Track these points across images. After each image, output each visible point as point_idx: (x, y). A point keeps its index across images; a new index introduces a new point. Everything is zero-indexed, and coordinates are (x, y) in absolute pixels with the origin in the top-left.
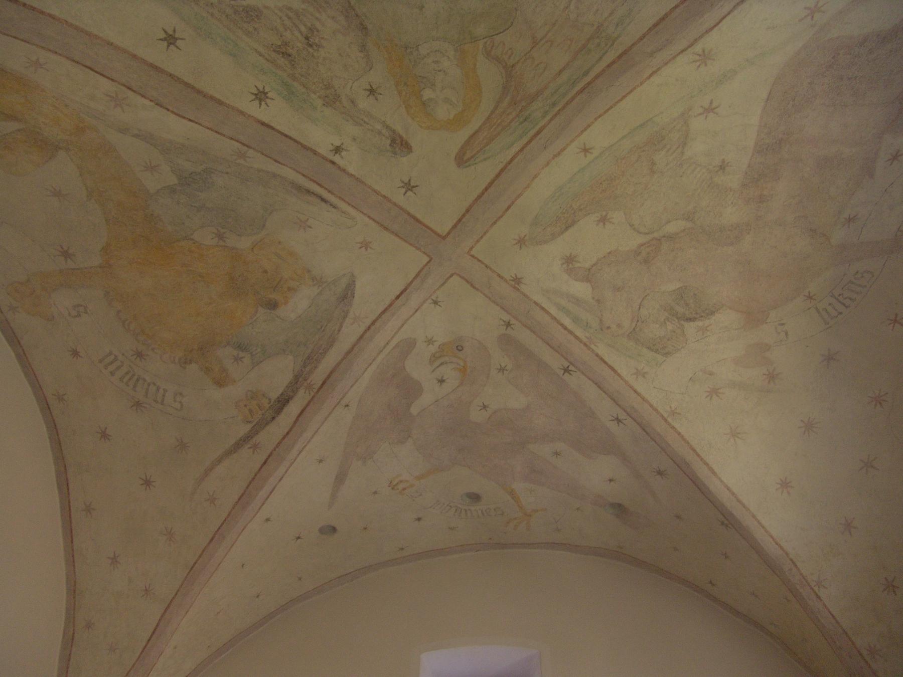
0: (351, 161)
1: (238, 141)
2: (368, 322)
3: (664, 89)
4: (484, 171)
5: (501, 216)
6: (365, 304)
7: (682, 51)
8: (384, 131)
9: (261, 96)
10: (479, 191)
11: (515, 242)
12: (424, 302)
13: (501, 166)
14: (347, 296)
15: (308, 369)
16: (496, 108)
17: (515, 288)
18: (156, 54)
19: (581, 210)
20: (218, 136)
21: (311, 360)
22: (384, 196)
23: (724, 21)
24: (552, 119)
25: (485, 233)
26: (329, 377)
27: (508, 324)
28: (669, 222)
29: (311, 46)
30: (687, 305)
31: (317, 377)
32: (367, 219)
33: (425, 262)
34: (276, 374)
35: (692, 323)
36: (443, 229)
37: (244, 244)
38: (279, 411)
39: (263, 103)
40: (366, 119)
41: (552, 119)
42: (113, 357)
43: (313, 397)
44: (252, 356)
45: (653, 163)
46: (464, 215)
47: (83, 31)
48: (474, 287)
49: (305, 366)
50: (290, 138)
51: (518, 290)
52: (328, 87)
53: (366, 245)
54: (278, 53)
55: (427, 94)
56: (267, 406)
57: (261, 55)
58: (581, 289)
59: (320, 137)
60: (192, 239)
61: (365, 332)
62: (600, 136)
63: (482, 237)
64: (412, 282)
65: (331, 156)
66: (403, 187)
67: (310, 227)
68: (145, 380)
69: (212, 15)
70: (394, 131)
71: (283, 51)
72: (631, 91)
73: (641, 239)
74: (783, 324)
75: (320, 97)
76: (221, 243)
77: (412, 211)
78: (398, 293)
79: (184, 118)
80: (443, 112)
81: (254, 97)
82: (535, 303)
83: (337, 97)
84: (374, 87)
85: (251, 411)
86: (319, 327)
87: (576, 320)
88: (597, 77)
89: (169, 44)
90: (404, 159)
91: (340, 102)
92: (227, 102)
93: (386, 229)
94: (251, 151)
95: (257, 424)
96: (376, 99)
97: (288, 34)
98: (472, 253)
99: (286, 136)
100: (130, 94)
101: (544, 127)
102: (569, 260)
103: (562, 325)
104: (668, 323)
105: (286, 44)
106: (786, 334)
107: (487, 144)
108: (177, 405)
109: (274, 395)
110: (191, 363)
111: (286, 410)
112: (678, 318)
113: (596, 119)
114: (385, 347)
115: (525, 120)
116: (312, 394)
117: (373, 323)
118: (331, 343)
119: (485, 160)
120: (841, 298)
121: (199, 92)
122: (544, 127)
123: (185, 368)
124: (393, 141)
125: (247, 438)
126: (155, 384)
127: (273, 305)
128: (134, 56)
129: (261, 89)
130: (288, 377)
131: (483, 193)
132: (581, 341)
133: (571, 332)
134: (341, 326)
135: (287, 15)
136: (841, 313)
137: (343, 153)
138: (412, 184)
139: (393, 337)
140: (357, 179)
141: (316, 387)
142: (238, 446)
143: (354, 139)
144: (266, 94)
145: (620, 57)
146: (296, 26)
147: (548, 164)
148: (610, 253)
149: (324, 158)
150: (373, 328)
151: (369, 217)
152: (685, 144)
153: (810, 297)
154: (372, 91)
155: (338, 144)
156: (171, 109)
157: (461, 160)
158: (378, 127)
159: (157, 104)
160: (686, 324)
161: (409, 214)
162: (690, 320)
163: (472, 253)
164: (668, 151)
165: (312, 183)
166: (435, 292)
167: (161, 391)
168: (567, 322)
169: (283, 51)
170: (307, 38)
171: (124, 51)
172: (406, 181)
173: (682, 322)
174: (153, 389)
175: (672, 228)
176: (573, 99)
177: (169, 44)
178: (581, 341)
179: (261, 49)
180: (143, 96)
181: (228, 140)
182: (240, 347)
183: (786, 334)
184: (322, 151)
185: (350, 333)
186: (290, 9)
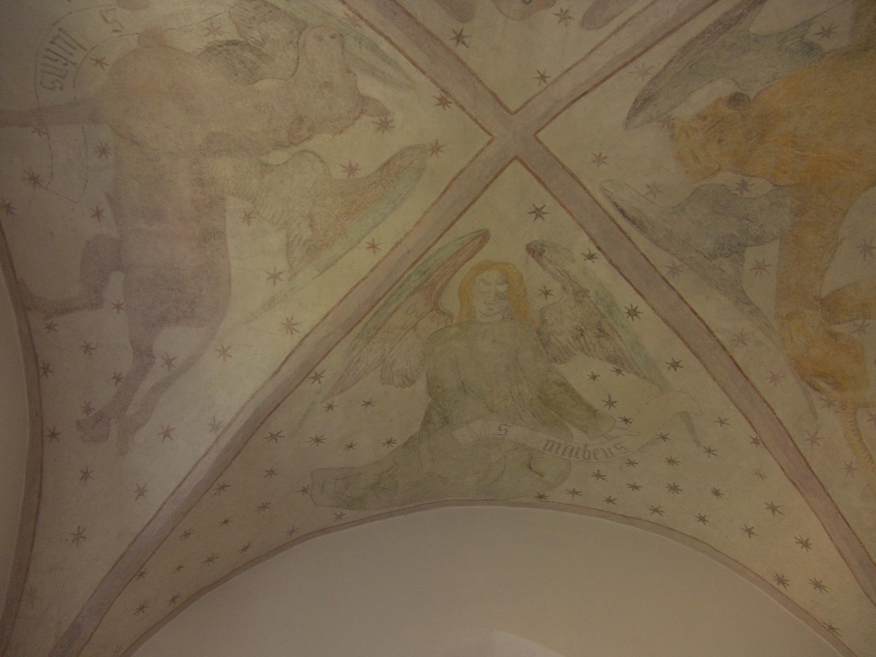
0: (583, 244)
1: (670, 285)
2: (631, 68)
3: (316, 299)
4: (465, 227)
5: (454, 179)
6: (629, 85)
7: (307, 336)
10: (473, 207)
11: (442, 149)
12: (556, 80)
13: (449, 232)
14: (644, 101)
16: (449, 280)
17: (446, 93)
19: (375, 183)
21: (726, 24)
22: (564, 207)
23: (283, 359)
24: (403, 276)
25: (472, 161)
27: (459, 38)
28: (285, 163)
29: (581, 330)
30: (242, 62)
32: (589, 188)
33: (543, 133)
35: (230, 38)
36: (517, 165)
37: (728, 178)
40: (558, 274)
41: (403, 276)
45: (311, 226)
46: (491, 182)
48: (494, 94)
50: (625, 278)
51: (443, 90)
53: (599, 159)
54: (606, 334)
55: (503, 288)
58: (371, 88)
59: (601, 270)
60: (776, 186)
61: (639, 55)
62: (361, 261)
63: (477, 156)
64: (563, 110)
67: (648, 186)
70: (538, 261)
71: (602, 333)
72: (341, 301)
73: (310, 145)
74: (116, 31)
76: (746, 179)
77: (542, 188)
78: (583, 98)
79: (699, 318)
80: (493, 275)
82: (423, 72)
87: (375, 48)
88: (368, 312)
89: (677, 363)
90: (536, 238)
92: (660, 319)
93: (572, 175)
94: (664, 274)
97: (594, 341)
98: (489, 138)
99: (628, 281)
100: (726, 344)
101: (410, 268)
102: (385, 126)
103: (391, 43)
104: (260, 39)
106: (105, 20)
107: (459, 251)
112: (248, 45)
113: (366, 277)
115: (425, 272)
117: (625, 65)
118: (685, 49)
119: (463, 237)
120: (64, 62)
122: (410, 268)
124: (540, 254)
127: (736, 100)
131: (469, 206)
132: (366, 21)
133: (381, 33)
134: (666, 67)
136: (52, 42)
137: (588, 253)
138: (534, 215)
139: (609, 37)
140: (583, 228)
144: (629, 313)
145: (352, 329)
147: (407, 235)
148: (341, 132)
150: (628, 59)
151: (585, 189)
152: (287, 245)
153: (99, 62)
154: (547, 293)
157: (484, 236)
158: (550, 266)
159: (712, 333)
160: (237, 37)
161: (545, 187)
162: (234, 43)
163: (489, 138)
164: (301, 239)
166: (540, 93)
168: (385, 46)
169: (602, 333)
170: (582, 335)
171: (709, 372)
172: (539, 219)
173: (242, 39)
175: (279, 157)
176: (385, 294)
178: (366, 21)
180: (718, 341)
182: (810, 48)
183: (105, 20)
185: (657, 59)
186: (586, 354)
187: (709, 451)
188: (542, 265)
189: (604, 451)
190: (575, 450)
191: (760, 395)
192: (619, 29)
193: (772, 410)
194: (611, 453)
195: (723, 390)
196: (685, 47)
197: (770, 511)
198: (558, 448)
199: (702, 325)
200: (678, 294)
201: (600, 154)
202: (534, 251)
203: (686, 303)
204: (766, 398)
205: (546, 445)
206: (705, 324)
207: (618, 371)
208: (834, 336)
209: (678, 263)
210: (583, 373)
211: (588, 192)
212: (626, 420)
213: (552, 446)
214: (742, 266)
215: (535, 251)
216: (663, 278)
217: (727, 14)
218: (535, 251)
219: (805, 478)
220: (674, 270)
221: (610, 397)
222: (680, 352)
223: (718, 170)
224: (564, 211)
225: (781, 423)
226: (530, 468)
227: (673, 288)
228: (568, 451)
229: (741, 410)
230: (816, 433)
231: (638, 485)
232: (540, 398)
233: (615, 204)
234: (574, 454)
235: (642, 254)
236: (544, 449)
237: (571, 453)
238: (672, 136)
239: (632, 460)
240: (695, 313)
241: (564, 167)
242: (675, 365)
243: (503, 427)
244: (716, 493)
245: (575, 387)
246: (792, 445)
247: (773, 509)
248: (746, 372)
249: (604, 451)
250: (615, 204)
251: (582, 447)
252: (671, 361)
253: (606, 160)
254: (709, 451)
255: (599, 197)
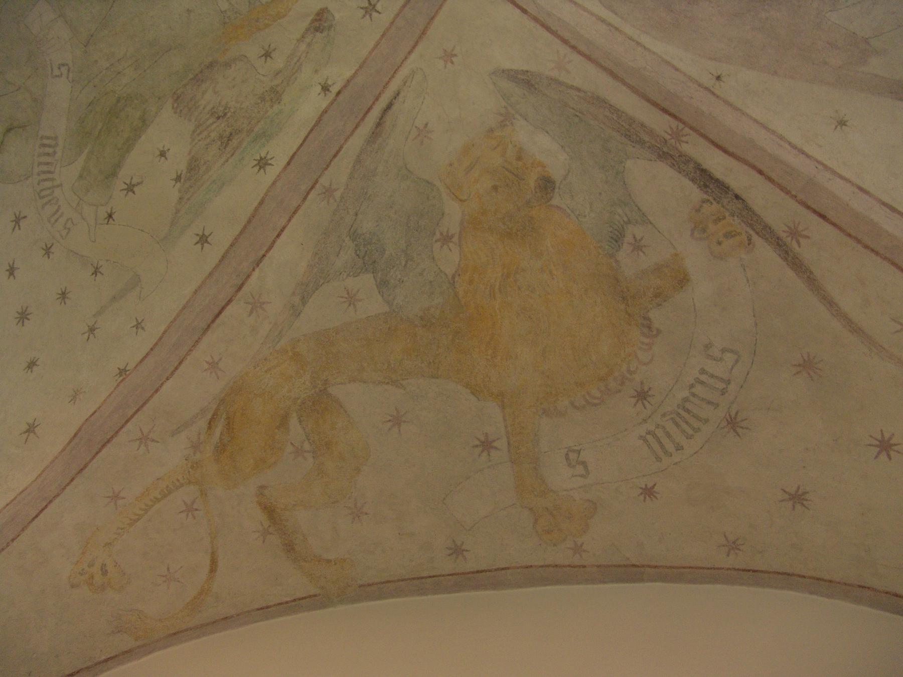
0: (338, 73)
1: (308, 193)
2: (564, 49)
8: (307, 40)
9: (262, 164)
14: (526, 81)
15: (646, 138)
18: (213, 254)
20: (300, 212)
21: (632, 131)
22: (383, 36)
26: (656, 105)
29: (225, 114)
31: (658, 122)
32: (413, 56)
34: (659, 188)
38: (724, 188)
39: (270, 162)
40: (295, 59)
42: (649, 437)
43: (691, 128)
44: (629, 222)
47: (181, 311)
49: (642, 143)
50: (307, 137)
52: (263, 99)
53: (449, 57)
56: (715, 207)
57: (227, 161)
59: (308, 105)
60: (453, 277)
61: (580, 53)
65: (331, 96)
66: (371, 15)
68: (686, 400)
69: (188, 199)
70: (307, 30)
71: (226, 140)
75: (272, 107)
76: (456, 239)
78: (518, 11)
79: (274, 242)
81: (262, 170)
83: (273, 90)
84: (263, 52)
85: (729, 235)
86: (577, 120)
89: (207, 241)
90: (337, 16)
91: (277, 86)
92: (262, 195)
93: (424, 33)
94: (321, 181)
95: (751, 226)
96: (274, 50)
97: (214, 135)
99: (304, 141)
100: (245, 289)
105: (221, 137)
108: (729, 358)
109: (695, 194)
110: (649, 319)
111: (718, 174)
114: (609, 25)
116: (687, 130)
117: (565, 41)
118: (599, 101)
121: (249, 222)
123: (659, 331)
124: (317, 29)
125: (779, 244)
126: (692, 386)
127: (547, 185)
128: (211, 274)
129: (256, 162)
130: (664, 171)
134: (572, 87)
135: (199, 135)
137: (330, 82)
139: (592, 14)
140: (361, 67)
141: (674, 123)
142: (797, 265)
143: (316, 71)
146: (209, 126)
149: (332, 103)
150: (573, 42)
151: (410, 53)
154: (267, 55)
155: (320, 88)
156: (263, 252)
158: (303, 47)
165: (367, 119)
167: (703, 378)
169: (226, 140)
170: (218, 118)
171: (203, 283)
174: (698, 389)
177: (207, 241)
179: (223, 159)
180: (249, 276)
181: (307, 203)
182: (617, 238)
184: (324, 105)
185: (580, 74)
186: (194, 132)
187: (92, 330)
188: (303, 37)
189: (57, 211)
190: (50, 176)
191: (187, 354)
192: (603, 21)
193: (172, 373)
194: (56, 221)
195: (184, 308)
196: (598, 98)
197: (24, 427)
198: (48, 154)
199: (265, 249)
200: (299, 207)
201: (455, 55)
202: (320, 20)
203: (289, 220)
204: (186, 362)
205: (48, 138)
206: (267, 251)
207: (178, 179)
208: (283, 422)
209: (338, 194)
210: (168, 137)
211: (406, 58)
212: (110, 216)
213: (50, 146)
214: (348, 275)
215: (321, 22)
216: (316, 182)
217: (643, 125)
218: (321, 22)
219: (89, 445)
220: (328, 192)
221: (138, 184)
222: (222, 238)
223: (461, 200)
224: (378, 36)
225: (157, 391)
226: (9, 130)
227: (305, 199)
228: (45, 168)
229: (160, 339)
230: (153, 440)
231: (16, 273)
232: (118, 101)
233: (398, 94)
234: (43, 177)
235: (341, 148)
236: (42, 138)
237: (44, 172)
238: (492, 130)
239: (52, 250)
240: (278, 236)
241: (432, 18)
242: (203, 240)
243: (64, 70)
244: (32, 365)
245: (143, 137)
246: (130, 413)
247: (31, 429)
248: (214, 325)
249: (57, 211)
250: (398, 94)
251: (56, 183)
252: (207, 233)
253: (449, 64)
254: (92, 330)
255: (404, 72)
